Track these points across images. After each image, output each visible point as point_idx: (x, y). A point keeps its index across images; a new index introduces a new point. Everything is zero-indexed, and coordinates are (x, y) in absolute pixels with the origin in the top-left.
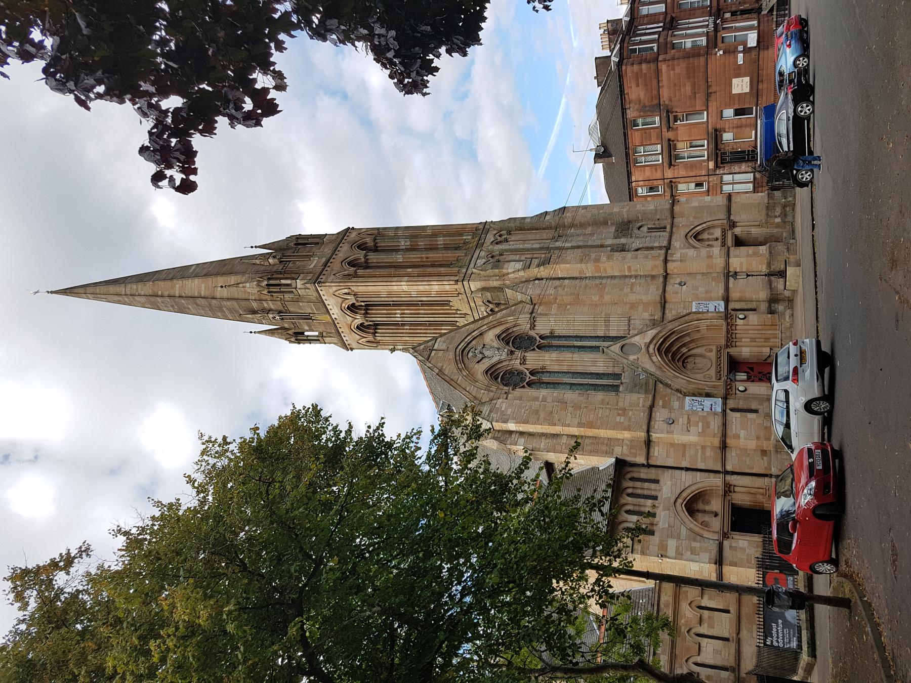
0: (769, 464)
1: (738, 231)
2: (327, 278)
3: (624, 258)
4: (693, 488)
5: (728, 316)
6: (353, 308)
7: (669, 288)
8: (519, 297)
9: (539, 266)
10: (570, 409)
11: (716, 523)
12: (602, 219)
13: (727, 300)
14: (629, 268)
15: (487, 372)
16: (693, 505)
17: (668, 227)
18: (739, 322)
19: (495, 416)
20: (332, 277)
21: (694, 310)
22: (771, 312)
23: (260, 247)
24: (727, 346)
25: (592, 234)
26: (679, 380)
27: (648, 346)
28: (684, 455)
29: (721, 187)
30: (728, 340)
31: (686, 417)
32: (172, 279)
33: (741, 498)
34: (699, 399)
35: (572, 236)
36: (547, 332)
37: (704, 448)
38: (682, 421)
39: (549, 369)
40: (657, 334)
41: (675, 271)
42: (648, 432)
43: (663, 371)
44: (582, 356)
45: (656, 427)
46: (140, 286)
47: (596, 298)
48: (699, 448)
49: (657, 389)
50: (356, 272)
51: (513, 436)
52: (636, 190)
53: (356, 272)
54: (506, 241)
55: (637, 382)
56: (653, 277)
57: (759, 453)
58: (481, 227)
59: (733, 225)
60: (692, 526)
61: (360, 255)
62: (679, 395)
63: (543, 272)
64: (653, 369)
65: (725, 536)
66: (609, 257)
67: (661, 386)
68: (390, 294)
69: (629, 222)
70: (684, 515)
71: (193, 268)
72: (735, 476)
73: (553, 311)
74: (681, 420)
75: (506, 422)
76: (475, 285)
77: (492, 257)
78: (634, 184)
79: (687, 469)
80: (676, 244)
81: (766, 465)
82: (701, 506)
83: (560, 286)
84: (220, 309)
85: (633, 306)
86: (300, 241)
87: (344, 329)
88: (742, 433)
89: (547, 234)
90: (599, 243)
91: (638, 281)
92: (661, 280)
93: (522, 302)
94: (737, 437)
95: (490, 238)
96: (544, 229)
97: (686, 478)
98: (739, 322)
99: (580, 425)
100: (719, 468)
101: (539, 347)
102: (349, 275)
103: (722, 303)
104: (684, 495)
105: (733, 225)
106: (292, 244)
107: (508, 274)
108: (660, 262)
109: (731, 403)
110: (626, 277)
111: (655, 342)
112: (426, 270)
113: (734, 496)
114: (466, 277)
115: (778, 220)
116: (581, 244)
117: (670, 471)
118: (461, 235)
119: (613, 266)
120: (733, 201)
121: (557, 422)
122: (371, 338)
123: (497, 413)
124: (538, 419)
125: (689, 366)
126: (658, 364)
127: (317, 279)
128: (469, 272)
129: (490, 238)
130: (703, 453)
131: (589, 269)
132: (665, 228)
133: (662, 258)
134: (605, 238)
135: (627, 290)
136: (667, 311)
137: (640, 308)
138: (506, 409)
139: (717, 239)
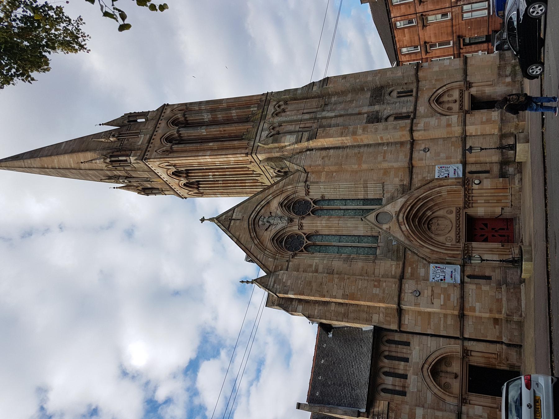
0: (501, 332)
1: (473, 91)
2: (151, 155)
3: (376, 130)
4: (437, 354)
5: (465, 182)
6: (177, 174)
7: (415, 155)
8: (296, 167)
9: (308, 140)
10: (336, 280)
11: (456, 385)
12: (359, 87)
13: (464, 164)
14: (381, 138)
15: (273, 239)
16: (436, 369)
17: (414, 90)
18: (475, 187)
19: (278, 287)
20: (155, 153)
21: (436, 177)
22: (503, 175)
23: (108, 124)
24: (465, 208)
25: (351, 101)
26: (425, 249)
27: (398, 215)
28: (429, 324)
29: (462, 16)
30: (465, 202)
31: (430, 289)
32: (51, 156)
33: (477, 360)
34: (441, 266)
35: (335, 104)
36: (319, 197)
37: (445, 316)
38: (427, 293)
39: (320, 233)
40: (406, 202)
41: (420, 138)
42: (399, 304)
43: (410, 241)
44: (346, 222)
45: (405, 300)
46: (32, 160)
47: (355, 167)
48: (442, 316)
49: (407, 255)
50: (171, 148)
51: (294, 303)
52: (395, 24)
53: (171, 148)
54: (284, 111)
55: (390, 248)
56: (402, 144)
57: (492, 322)
58: (264, 98)
59: (469, 85)
60: (436, 391)
61: (174, 131)
62: (424, 262)
63: (312, 144)
64: (402, 238)
65: (464, 401)
66: (364, 129)
67: (409, 252)
68: (200, 164)
69: (382, 87)
70: (429, 380)
71: (64, 145)
72: (472, 342)
73: (323, 179)
74: (426, 291)
75: (286, 293)
76: (261, 157)
77: (273, 129)
78: (393, 20)
79: (432, 335)
80: (422, 109)
81: (498, 334)
82: (444, 368)
83: (327, 156)
84: (88, 175)
85: (386, 172)
86: (131, 119)
87: (177, 189)
88: (478, 306)
89: (314, 103)
90: (356, 111)
91: (390, 148)
92: (409, 146)
93: (298, 170)
94: (473, 309)
95: (271, 109)
96: (313, 98)
97: (432, 343)
98: (475, 187)
99: (344, 297)
100: (458, 335)
101: (313, 212)
102: (167, 151)
103: (460, 166)
104: (430, 360)
105: (469, 85)
106: (126, 122)
107: (285, 146)
108: (406, 133)
109: (469, 271)
110: (379, 144)
111: (403, 210)
112: (224, 142)
113: (471, 358)
114: (253, 151)
115: (509, 79)
116: (342, 113)
117: (418, 336)
118: (249, 107)
119: (367, 137)
120: (468, 65)
121: (326, 293)
122: (196, 191)
123: (279, 285)
124: (311, 290)
125: (433, 228)
126: (406, 233)
127: (143, 158)
128: (256, 145)
129: (271, 109)
130: (445, 322)
131: (348, 140)
132: (412, 91)
133: (408, 129)
134: (362, 106)
135: (380, 158)
136: (414, 176)
137: (392, 173)
138: (287, 280)
139: (456, 101)
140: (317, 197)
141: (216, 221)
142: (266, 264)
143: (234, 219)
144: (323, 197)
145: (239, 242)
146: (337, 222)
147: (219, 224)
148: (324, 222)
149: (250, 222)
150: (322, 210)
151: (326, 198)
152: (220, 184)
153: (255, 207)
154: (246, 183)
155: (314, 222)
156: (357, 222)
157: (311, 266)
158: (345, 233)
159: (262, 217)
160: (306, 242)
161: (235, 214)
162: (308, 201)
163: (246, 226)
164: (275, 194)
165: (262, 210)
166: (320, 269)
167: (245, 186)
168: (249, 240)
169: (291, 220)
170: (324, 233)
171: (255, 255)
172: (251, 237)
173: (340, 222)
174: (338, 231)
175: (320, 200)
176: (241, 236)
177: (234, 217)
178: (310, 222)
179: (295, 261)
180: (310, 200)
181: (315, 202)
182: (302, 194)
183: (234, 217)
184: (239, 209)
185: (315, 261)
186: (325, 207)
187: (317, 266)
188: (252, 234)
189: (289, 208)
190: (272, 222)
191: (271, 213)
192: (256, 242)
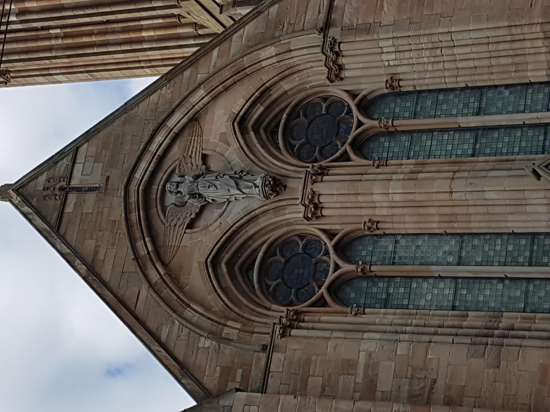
101: (360, 146)
140: (373, 84)
141: (17, 199)
142: (190, 361)
143: (78, 190)
144: (393, 81)
145: (94, 277)
146: (444, 186)
147: (26, 209)
148: (395, 187)
149: (133, 199)
150: (392, 134)
151: (407, 86)
152: (57, 37)
153: (146, 138)
154: (141, 29)
155: (361, 187)
156: (518, 184)
157: (349, 366)
158: (476, 227)
159: (176, 178)
160: (337, 267)
161: (78, 167)
162: (342, 102)
163: (119, 213)
164: (215, 82)
165: (176, 150)
166: (386, 381)
167: (141, 41)
168: (133, 267)
169: (276, 185)
170: (399, 228)
171: (153, 326)
172: (137, 258)
173: (458, 185)
174: (451, 218)
175: (383, 97)
176: (102, 252)
177: (75, 183)
178: (345, 188)
179: (295, 346)
180: (345, 97)
181: (367, 105)
182: (314, 75)
183: (75, 183)
184: (93, 149)
185: (364, 346)
186: (402, 124)
187: (372, 365)
188: (140, 244)
189: (273, 134)
190: (210, 194)
191: (205, 157)
192: (154, 276)
